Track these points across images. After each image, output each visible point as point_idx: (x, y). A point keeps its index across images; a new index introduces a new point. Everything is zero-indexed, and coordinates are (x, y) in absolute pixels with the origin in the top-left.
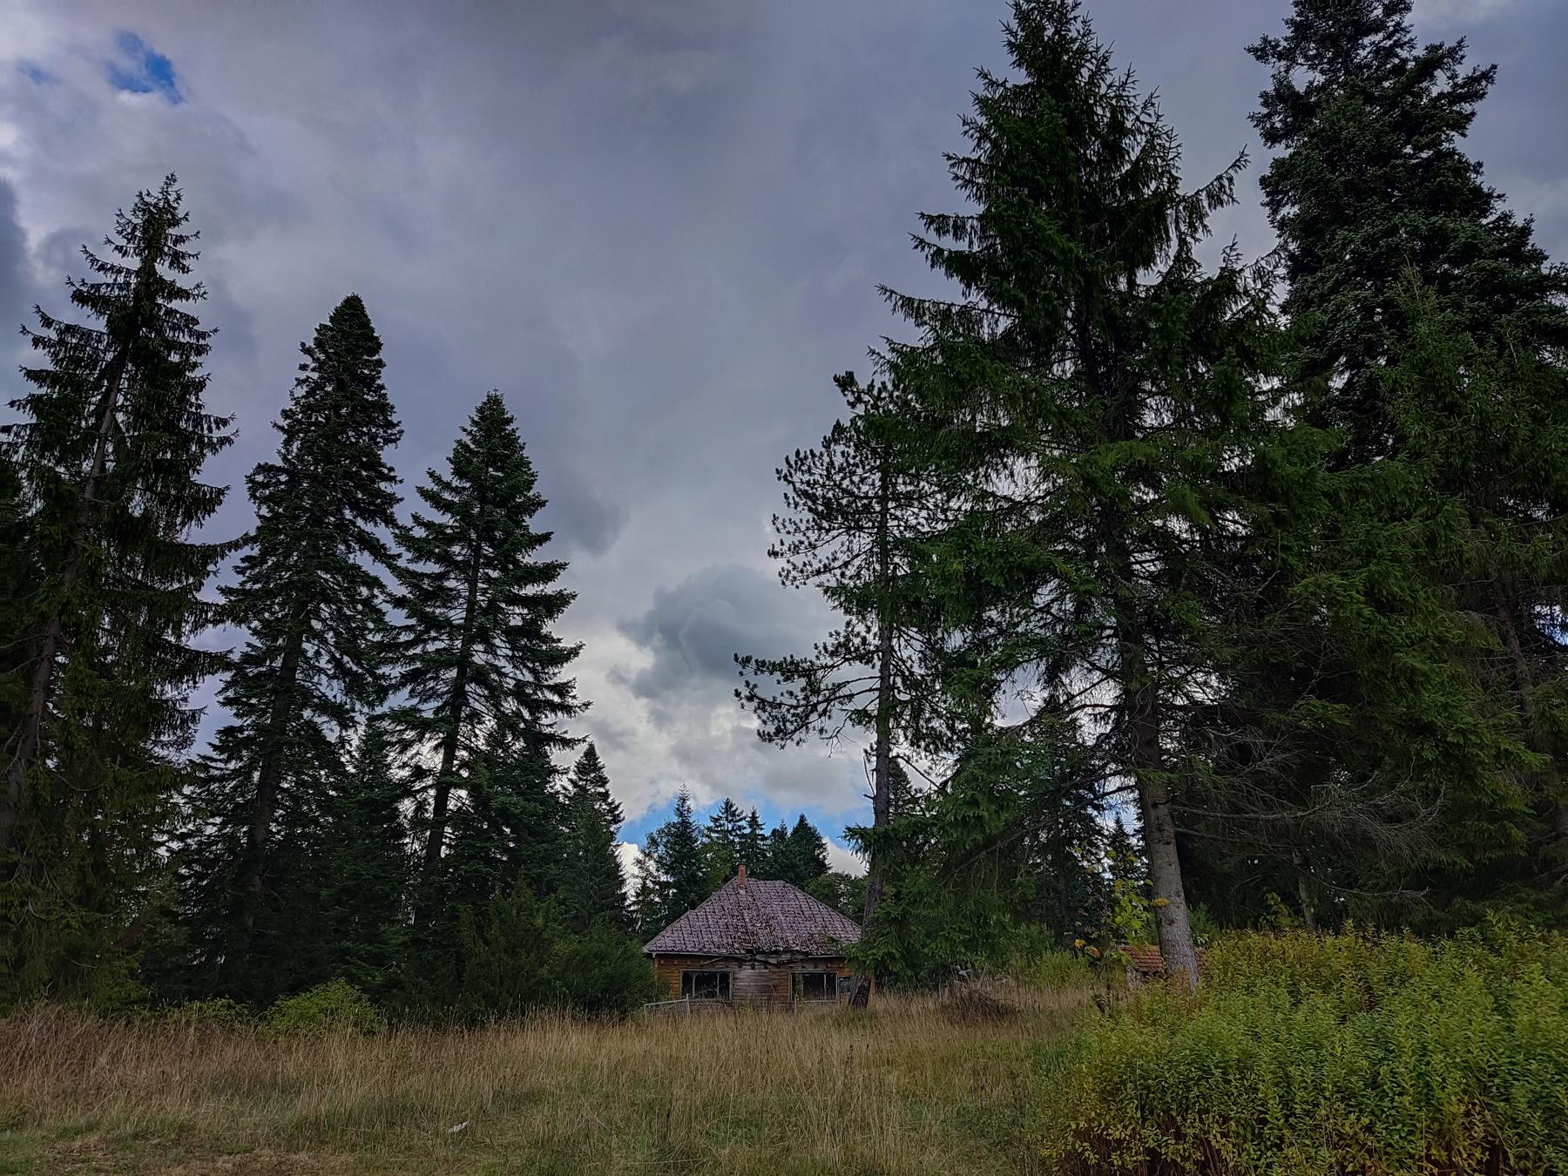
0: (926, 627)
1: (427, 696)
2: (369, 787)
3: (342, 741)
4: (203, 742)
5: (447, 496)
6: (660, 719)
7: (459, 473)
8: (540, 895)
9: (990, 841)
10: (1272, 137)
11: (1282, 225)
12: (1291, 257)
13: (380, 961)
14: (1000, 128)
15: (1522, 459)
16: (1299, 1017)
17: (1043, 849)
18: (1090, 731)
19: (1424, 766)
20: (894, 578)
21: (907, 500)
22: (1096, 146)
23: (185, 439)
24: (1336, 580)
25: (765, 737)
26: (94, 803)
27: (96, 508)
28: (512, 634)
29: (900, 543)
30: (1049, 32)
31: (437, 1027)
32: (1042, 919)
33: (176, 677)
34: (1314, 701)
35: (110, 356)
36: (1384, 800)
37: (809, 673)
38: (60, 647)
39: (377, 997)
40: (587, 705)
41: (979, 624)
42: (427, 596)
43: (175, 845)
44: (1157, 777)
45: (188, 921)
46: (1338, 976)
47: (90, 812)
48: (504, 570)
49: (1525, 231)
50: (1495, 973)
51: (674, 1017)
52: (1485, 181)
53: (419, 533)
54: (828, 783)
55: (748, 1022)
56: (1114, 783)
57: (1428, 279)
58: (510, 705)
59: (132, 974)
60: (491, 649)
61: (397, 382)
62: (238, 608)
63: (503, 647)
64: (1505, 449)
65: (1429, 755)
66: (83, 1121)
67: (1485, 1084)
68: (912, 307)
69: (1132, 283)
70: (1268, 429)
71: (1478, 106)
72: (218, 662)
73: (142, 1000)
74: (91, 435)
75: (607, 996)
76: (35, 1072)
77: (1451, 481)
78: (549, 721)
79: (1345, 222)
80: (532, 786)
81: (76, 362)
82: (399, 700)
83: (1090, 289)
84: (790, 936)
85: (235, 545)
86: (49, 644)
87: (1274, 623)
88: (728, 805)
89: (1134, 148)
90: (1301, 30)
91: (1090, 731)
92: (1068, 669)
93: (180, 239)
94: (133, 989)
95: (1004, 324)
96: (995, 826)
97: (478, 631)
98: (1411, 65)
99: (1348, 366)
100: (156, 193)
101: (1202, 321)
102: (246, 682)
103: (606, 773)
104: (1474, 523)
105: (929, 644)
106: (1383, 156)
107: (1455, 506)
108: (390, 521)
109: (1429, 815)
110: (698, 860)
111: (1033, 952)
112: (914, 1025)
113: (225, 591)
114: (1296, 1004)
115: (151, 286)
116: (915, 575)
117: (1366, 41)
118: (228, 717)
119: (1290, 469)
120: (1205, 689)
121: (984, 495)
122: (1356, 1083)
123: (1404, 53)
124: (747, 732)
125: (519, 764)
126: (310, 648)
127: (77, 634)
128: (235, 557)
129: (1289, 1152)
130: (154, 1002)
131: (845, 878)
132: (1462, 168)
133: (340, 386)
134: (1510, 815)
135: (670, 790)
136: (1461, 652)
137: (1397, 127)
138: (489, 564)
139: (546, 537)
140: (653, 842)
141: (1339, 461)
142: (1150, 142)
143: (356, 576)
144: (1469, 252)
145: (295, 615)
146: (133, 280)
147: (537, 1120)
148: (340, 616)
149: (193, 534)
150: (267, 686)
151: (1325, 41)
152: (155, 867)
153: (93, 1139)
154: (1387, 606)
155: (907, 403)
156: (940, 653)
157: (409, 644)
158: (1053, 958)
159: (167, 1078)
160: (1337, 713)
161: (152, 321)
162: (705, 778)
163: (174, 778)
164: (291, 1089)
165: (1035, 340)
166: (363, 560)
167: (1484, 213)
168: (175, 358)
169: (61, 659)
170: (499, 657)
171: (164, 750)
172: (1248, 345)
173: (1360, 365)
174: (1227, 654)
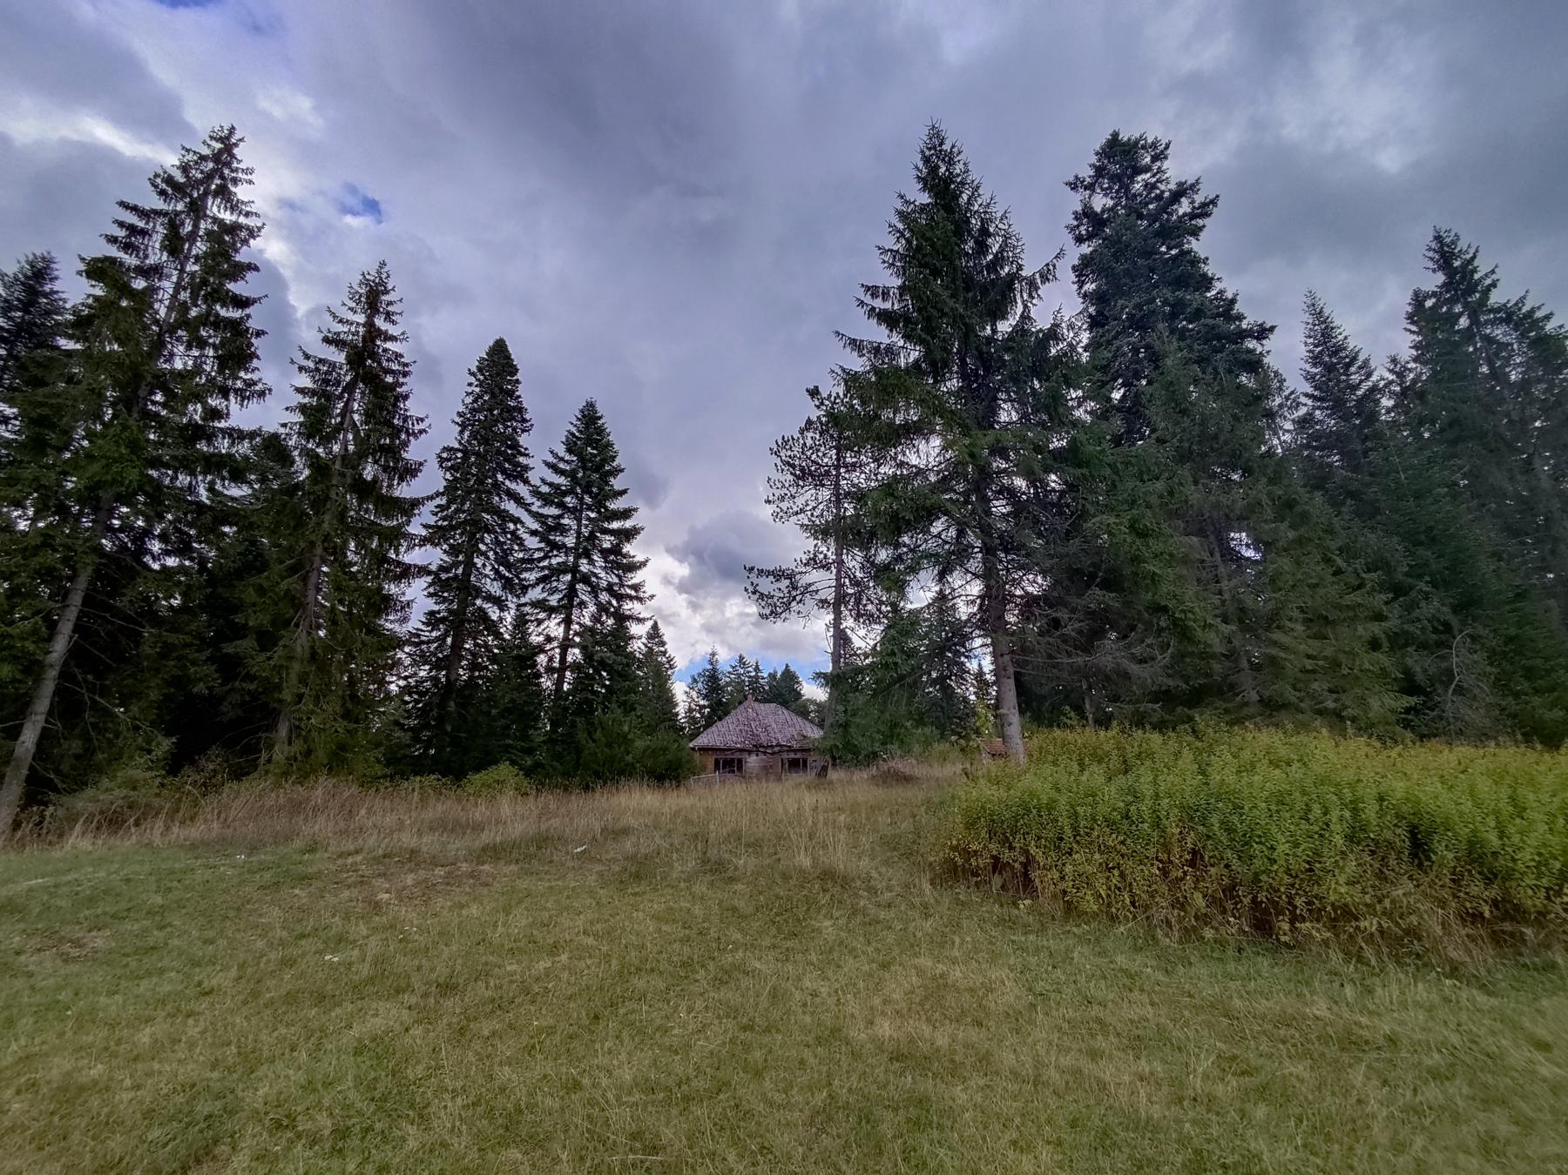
0: (865, 547)
1: (553, 591)
2: (519, 647)
3: (501, 619)
4: (416, 621)
5: (562, 465)
6: (695, 607)
7: (570, 451)
8: (626, 713)
9: (902, 678)
10: (1080, 240)
11: (1085, 296)
12: (1090, 316)
13: (530, 751)
14: (911, 231)
15: (1226, 443)
16: (1084, 778)
17: (934, 682)
18: (964, 611)
19: (1160, 630)
20: (844, 517)
21: (853, 467)
22: (971, 243)
23: (397, 431)
24: (1112, 520)
25: (763, 616)
26: (350, 657)
27: (343, 475)
28: (605, 553)
29: (847, 494)
30: (943, 169)
31: (566, 790)
32: (932, 724)
33: (398, 578)
34: (1097, 591)
35: (348, 378)
36: (1137, 650)
37: (790, 577)
38: (324, 562)
39: (529, 773)
40: (652, 597)
41: (897, 546)
42: (550, 529)
43: (402, 683)
44: (1004, 639)
45: (410, 729)
46: (1108, 754)
47: (347, 663)
48: (599, 512)
49: (1233, 301)
50: (1199, 751)
51: (709, 785)
52: (1209, 269)
53: (545, 489)
54: (806, 644)
55: (754, 787)
56: (978, 642)
57: (1172, 331)
58: (604, 597)
59: (379, 761)
60: (591, 562)
61: (527, 394)
62: (436, 536)
63: (599, 561)
64: (1216, 437)
65: (1163, 624)
66: (352, 848)
67: (1192, 816)
68: (856, 345)
69: (994, 331)
70: (1076, 424)
71: (1207, 221)
72: (423, 570)
73: (385, 777)
74: (339, 428)
75: (668, 771)
76: (322, 819)
77: (1183, 457)
78: (629, 607)
79: (1123, 294)
80: (619, 646)
81: (326, 382)
82: (535, 594)
83: (968, 334)
84: (779, 736)
85: (431, 498)
86: (317, 560)
87: (1075, 545)
88: (741, 658)
89: (995, 245)
90: (1100, 171)
91: (964, 611)
92: (951, 572)
93: (390, 303)
94: (379, 770)
95: (914, 355)
96: (904, 669)
97: (585, 549)
98: (1167, 194)
99: (1123, 385)
100: (373, 273)
101: (1035, 355)
102: (442, 583)
103: (665, 638)
104: (1196, 483)
105: (867, 559)
106: (1149, 253)
107: (1185, 472)
108: (526, 482)
109: (1164, 659)
110: (720, 693)
111: (927, 744)
112: (854, 787)
113: (426, 526)
114: (1082, 771)
115: (373, 333)
116: (858, 516)
117: (1139, 178)
118: (431, 605)
119: (1091, 448)
120: (1034, 584)
121: (901, 465)
122: (1116, 816)
123: (1163, 187)
124: (748, 615)
125: (611, 633)
126: (479, 561)
127: (334, 554)
128: (431, 505)
129: (1076, 856)
130: (392, 777)
131: (814, 702)
132: (1195, 261)
133: (493, 396)
134: (1213, 656)
135: (704, 649)
136: (1185, 561)
137: (1158, 234)
138: (589, 508)
139: (625, 492)
140: (695, 681)
141: (1117, 441)
142: (1005, 241)
143: (505, 517)
144: (1197, 314)
145: (470, 540)
146: (361, 329)
147: (628, 845)
148: (498, 543)
149: (404, 491)
150: (455, 586)
151: (1114, 178)
152: (388, 697)
153: (359, 858)
154: (1143, 534)
155: (852, 406)
156: (873, 563)
157: (540, 560)
158: (938, 747)
159: (406, 817)
160: (1111, 599)
161: (374, 356)
162: (723, 642)
163: (399, 643)
164: (478, 828)
165: (935, 366)
166: (510, 507)
167: (1208, 289)
168: (389, 379)
169: (325, 569)
170: (596, 566)
171: (390, 624)
172: (1065, 371)
173: (1131, 385)
174: (1048, 564)
